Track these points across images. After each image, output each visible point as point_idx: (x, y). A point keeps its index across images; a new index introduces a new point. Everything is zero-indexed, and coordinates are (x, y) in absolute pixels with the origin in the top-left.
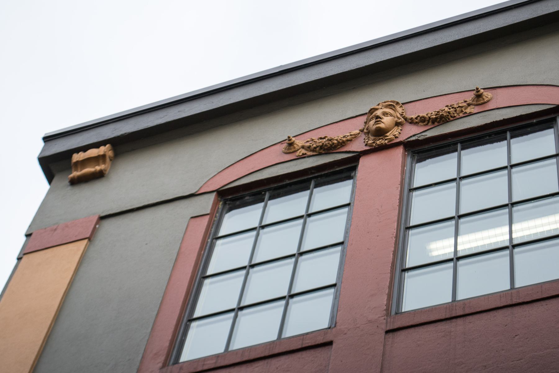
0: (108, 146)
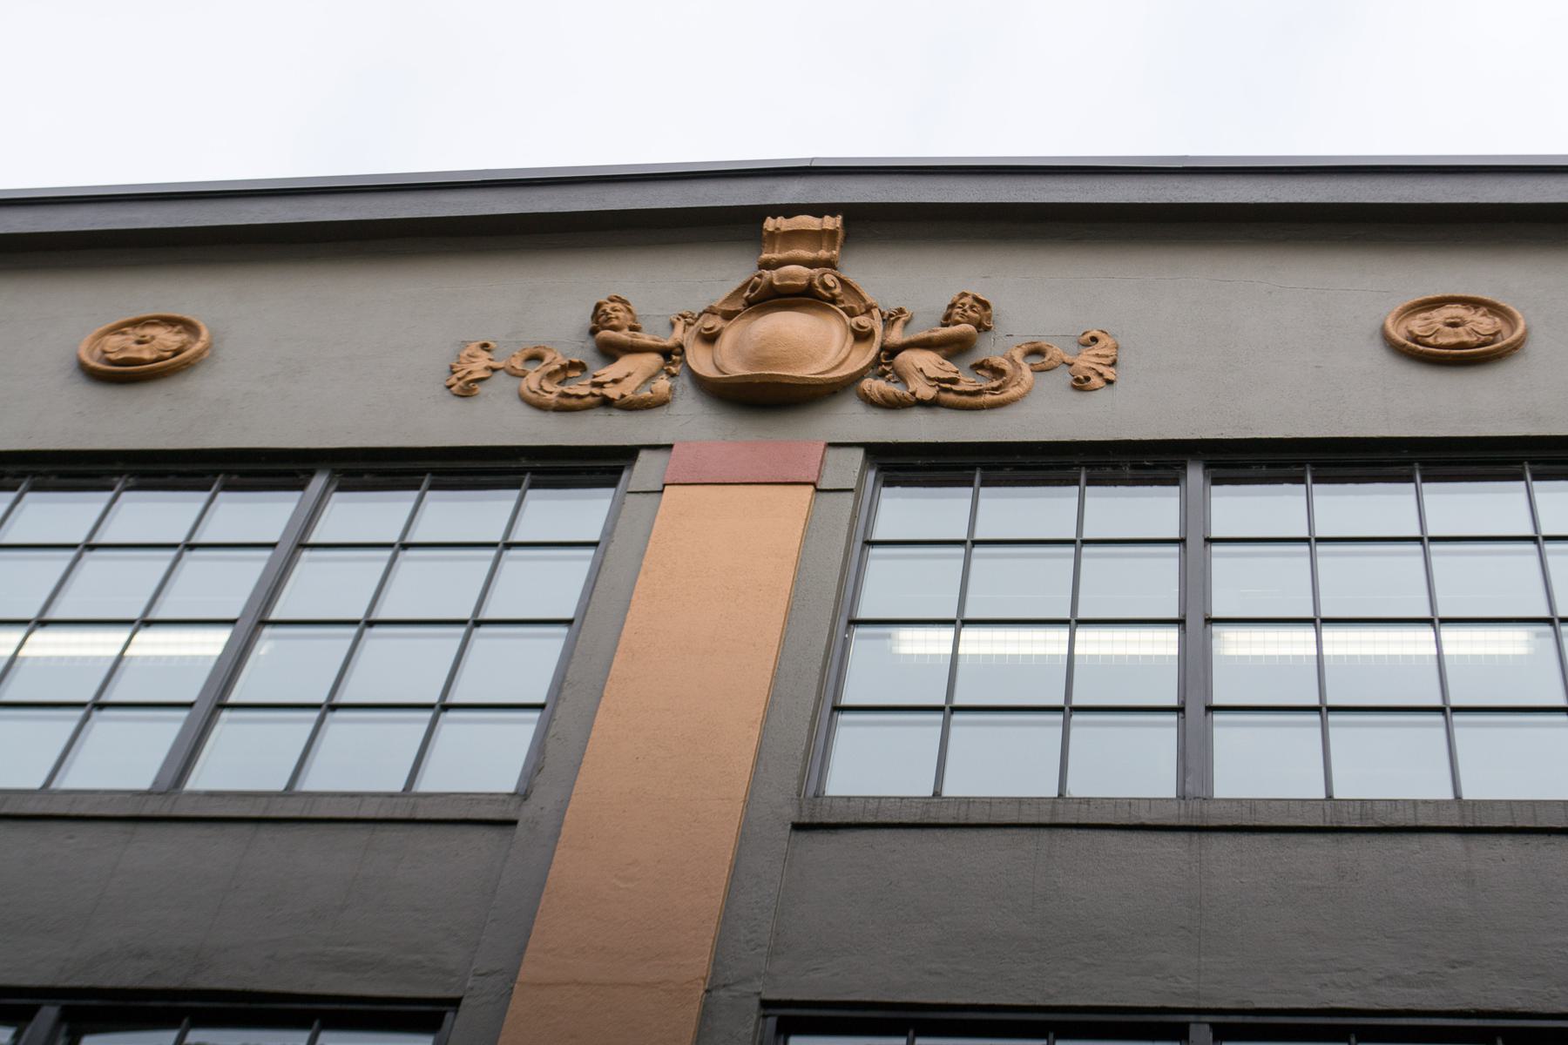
0: (840, 218)
